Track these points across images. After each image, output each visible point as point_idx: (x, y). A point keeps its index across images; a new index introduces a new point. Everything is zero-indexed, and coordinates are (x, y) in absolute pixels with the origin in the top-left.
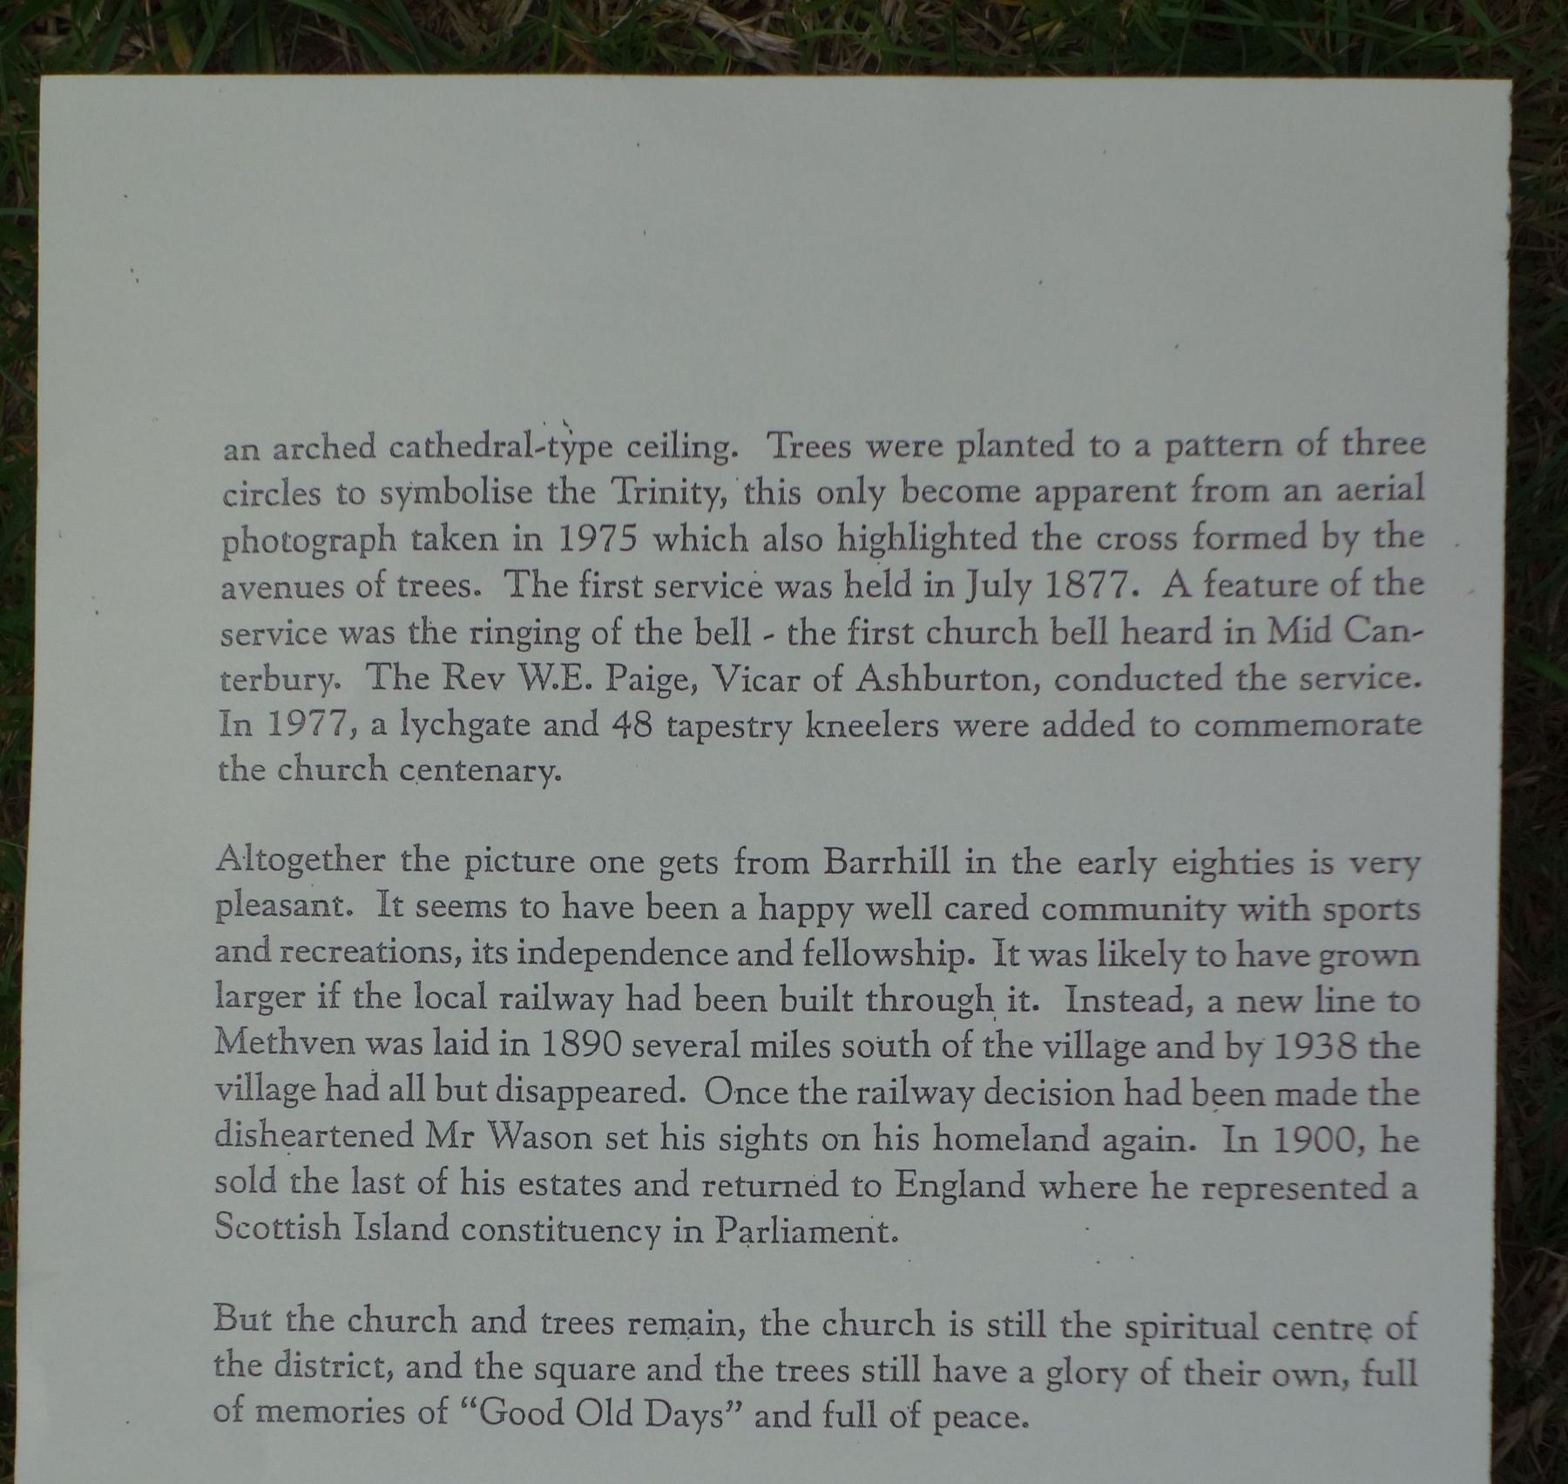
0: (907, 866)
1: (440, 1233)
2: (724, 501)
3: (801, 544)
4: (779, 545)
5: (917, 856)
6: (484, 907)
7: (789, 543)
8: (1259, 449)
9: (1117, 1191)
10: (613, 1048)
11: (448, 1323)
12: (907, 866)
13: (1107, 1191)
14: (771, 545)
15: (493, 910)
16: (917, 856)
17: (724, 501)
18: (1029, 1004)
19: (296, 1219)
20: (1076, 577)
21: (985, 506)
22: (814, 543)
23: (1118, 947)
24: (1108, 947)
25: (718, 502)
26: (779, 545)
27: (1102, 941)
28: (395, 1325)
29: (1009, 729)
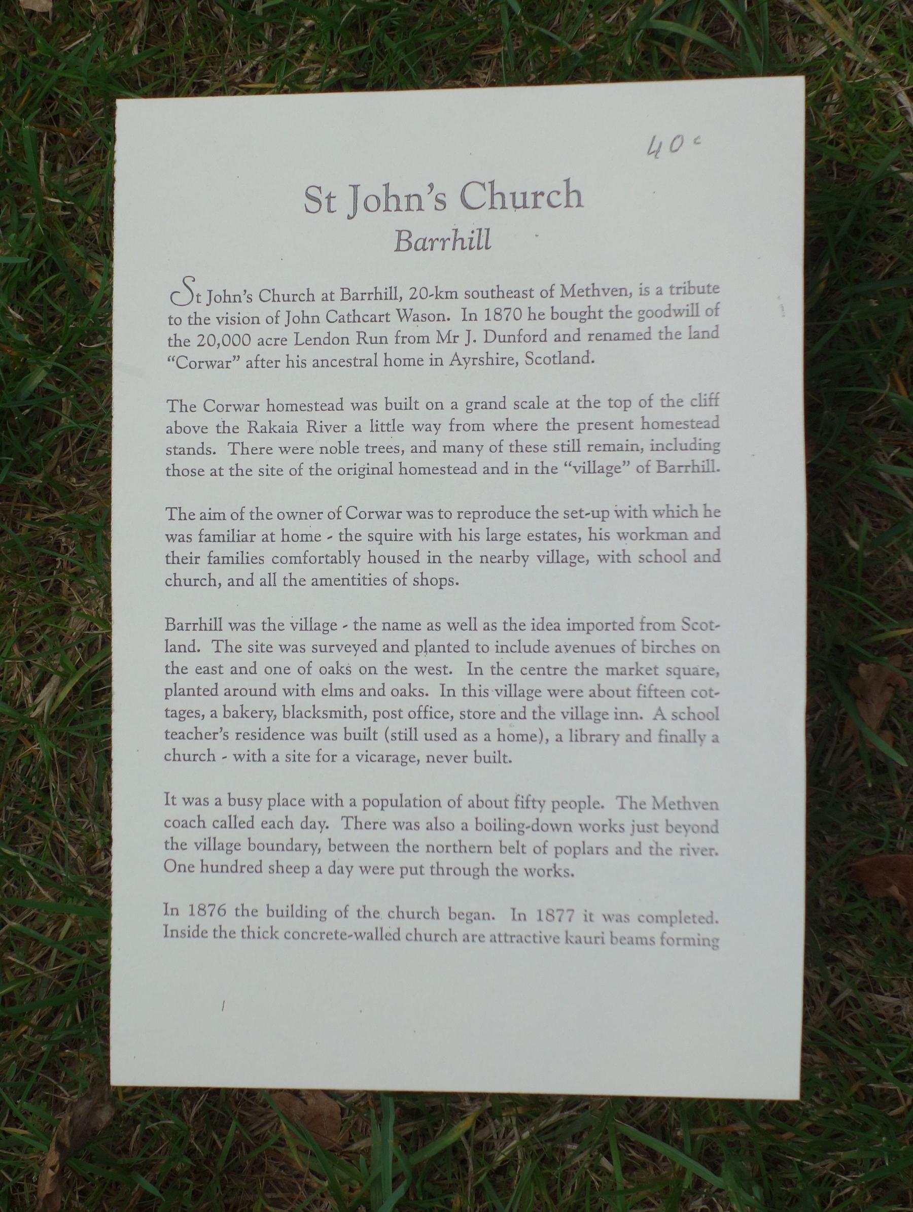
0: (378, 296)
1: (405, 649)
2: (320, 850)
3: (444, 827)
4: (434, 827)
5: (383, 291)
6: (343, 692)
7: (439, 826)
8: (482, 850)
9: (574, 694)
10: (246, 342)
11: (311, 297)
12: (378, 296)
13: (568, 694)
14: (429, 828)
15: (347, 693)
16: (383, 291)
17: (320, 850)
18: (507, 760)
19: (538, 934)
20: (498, 311)
21: (521, 743)
22: (450, 826)
23: (579, 733)
24: (574, 732)
25: (317, 851)
26: (434, 827)
27: (571, 730)
28: (286, 298)
29: (528, 427)
